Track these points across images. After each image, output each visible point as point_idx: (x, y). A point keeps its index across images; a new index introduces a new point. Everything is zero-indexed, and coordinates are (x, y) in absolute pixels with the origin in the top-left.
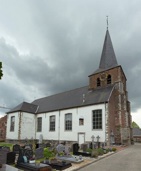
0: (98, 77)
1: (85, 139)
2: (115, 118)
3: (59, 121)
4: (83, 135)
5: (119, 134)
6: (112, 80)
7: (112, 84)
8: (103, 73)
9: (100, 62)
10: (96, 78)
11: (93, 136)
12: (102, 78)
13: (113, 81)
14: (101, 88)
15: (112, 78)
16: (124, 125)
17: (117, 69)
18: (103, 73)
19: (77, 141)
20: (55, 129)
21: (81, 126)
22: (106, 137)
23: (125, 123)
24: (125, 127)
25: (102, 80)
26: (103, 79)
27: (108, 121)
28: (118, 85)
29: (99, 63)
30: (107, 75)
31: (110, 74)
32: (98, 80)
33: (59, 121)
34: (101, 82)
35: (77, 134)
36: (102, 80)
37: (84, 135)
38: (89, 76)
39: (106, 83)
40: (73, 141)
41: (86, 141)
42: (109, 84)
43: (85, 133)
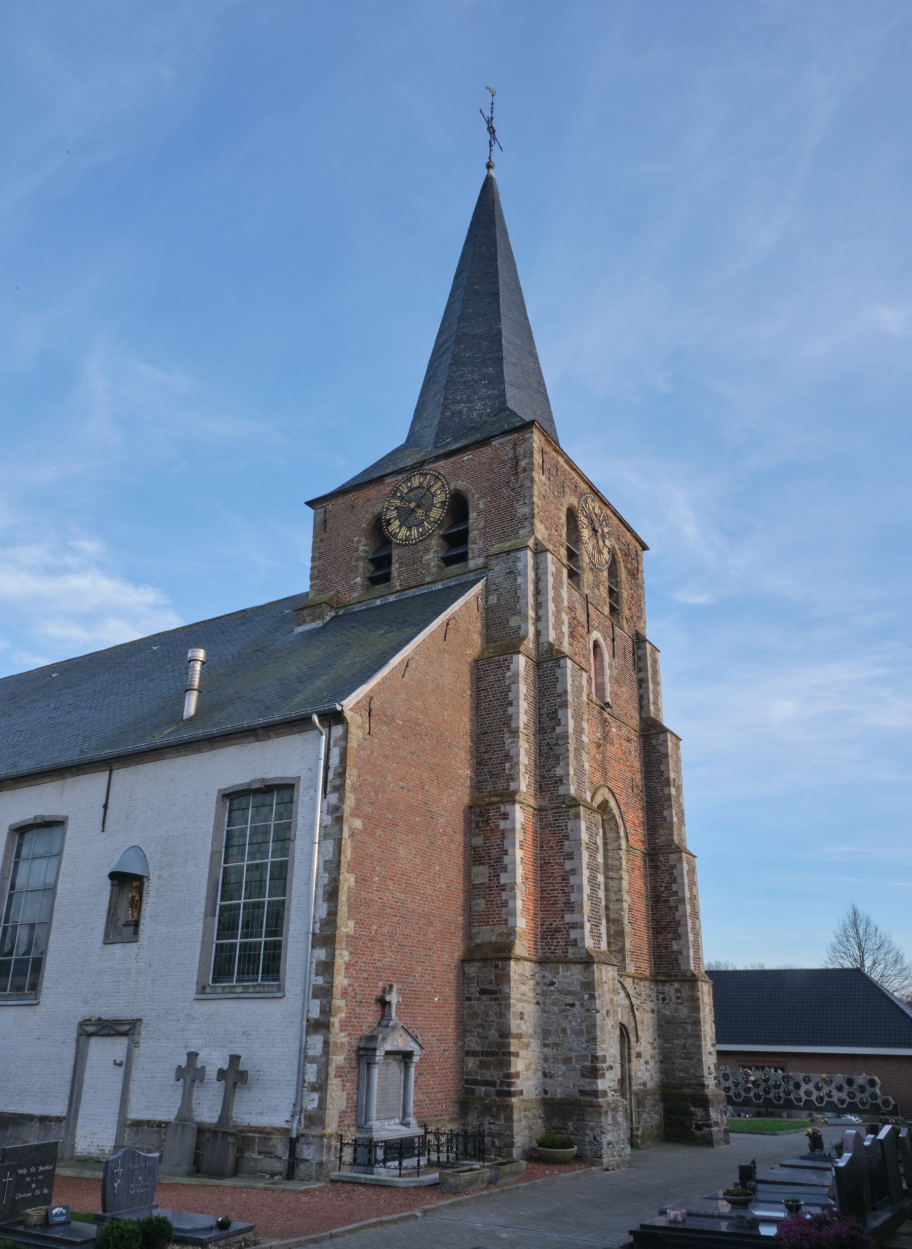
0: (378, 509)
1: (133, 1097)
2: (476, 869)
3: (105, 807)
4: (117, 1047)
5: (493, 1034)
6: (473, 534)
7: (472, 564)
8: (416, 482)
9: (421, 396)
10: (364, 519)
11: (192, 1056)
12: (406, 516)
13: (481, 544)
14: (392, 598)
15: (473, 515)
16: (560, 939)
17: (514, 448)
18: (416, 482)
19: (58, 1108)
20: (136, 924)
21: (117, 949)
22: (301, 1072)
23: (568, 918)
24: (566, 962)
25: (403, 533)
26: (410, 529)
27: (679, 850)
28: (512, 573)
29: (523, 291)
30: (440, 497)
31: (461, 484)
32: (378, 527)
33: (105, 807)
34: (396, 553)
35: (74, 1028)
36: (403, 533)
37: (124, 1040)
38: (310, 504)
39: (432, 556)
40: (30, 1118)
41: (136, 1113)
42: (454, 569)
43: (144, 1031)
